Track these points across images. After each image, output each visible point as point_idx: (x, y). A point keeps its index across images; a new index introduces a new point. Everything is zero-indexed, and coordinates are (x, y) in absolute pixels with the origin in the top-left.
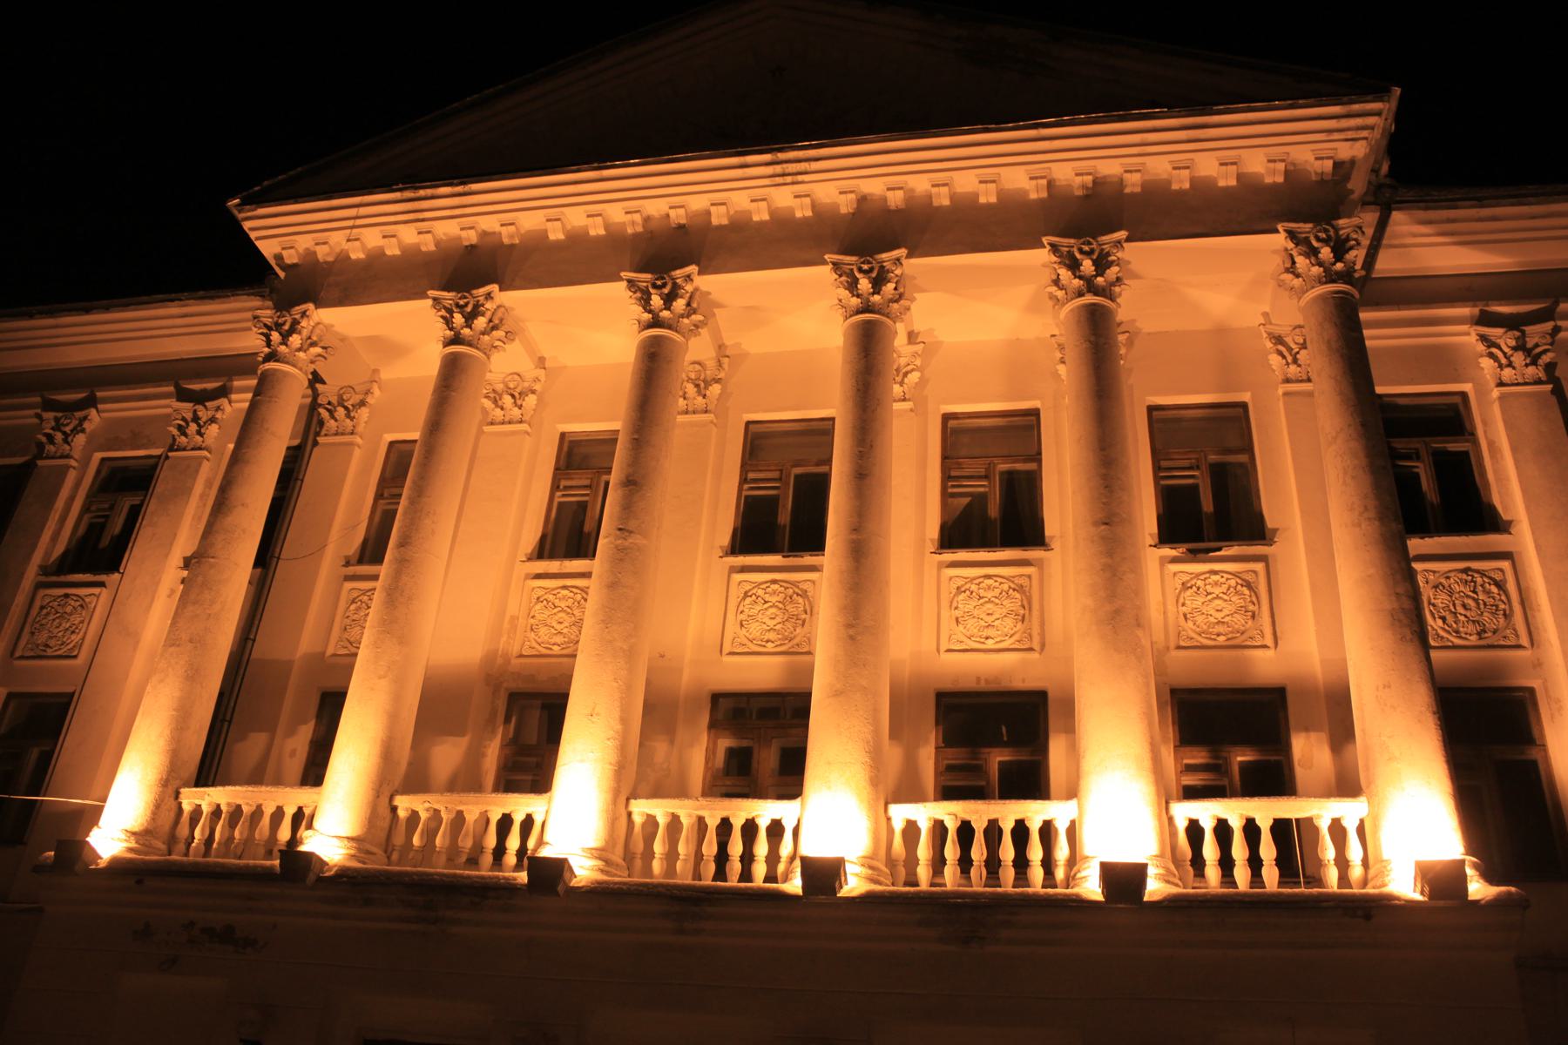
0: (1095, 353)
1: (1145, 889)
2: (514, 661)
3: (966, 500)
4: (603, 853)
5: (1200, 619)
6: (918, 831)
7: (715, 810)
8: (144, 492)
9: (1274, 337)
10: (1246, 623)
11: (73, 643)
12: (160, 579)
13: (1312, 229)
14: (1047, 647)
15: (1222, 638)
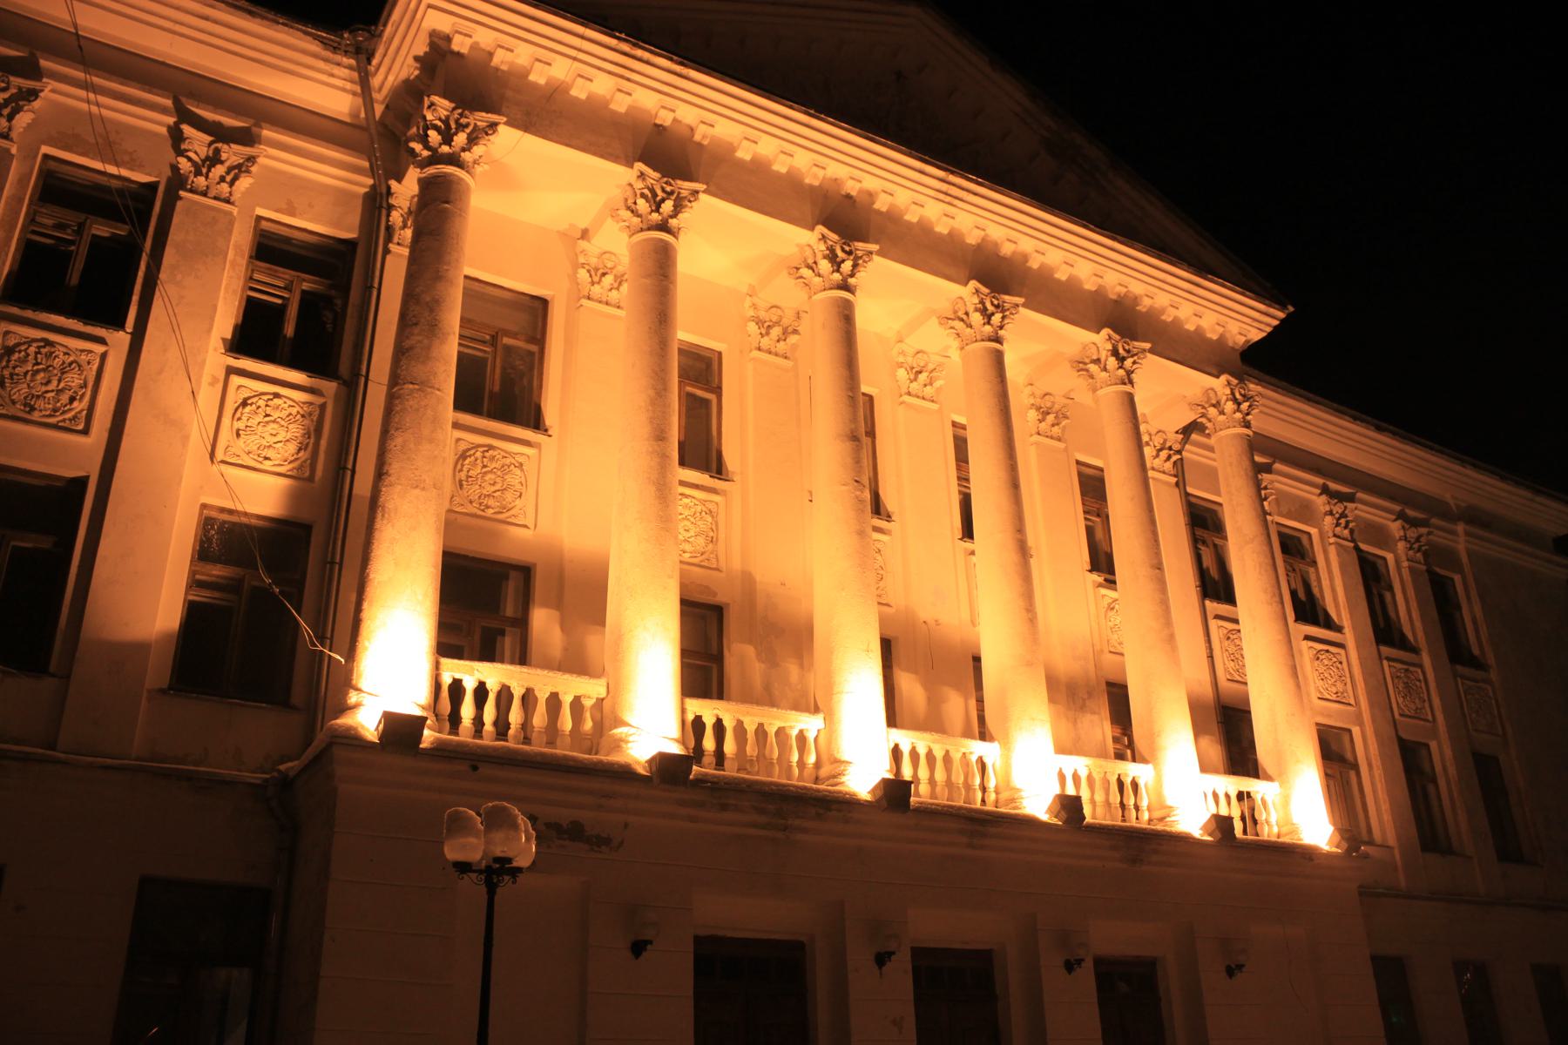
6: (703, 725)
11: (73, 413)
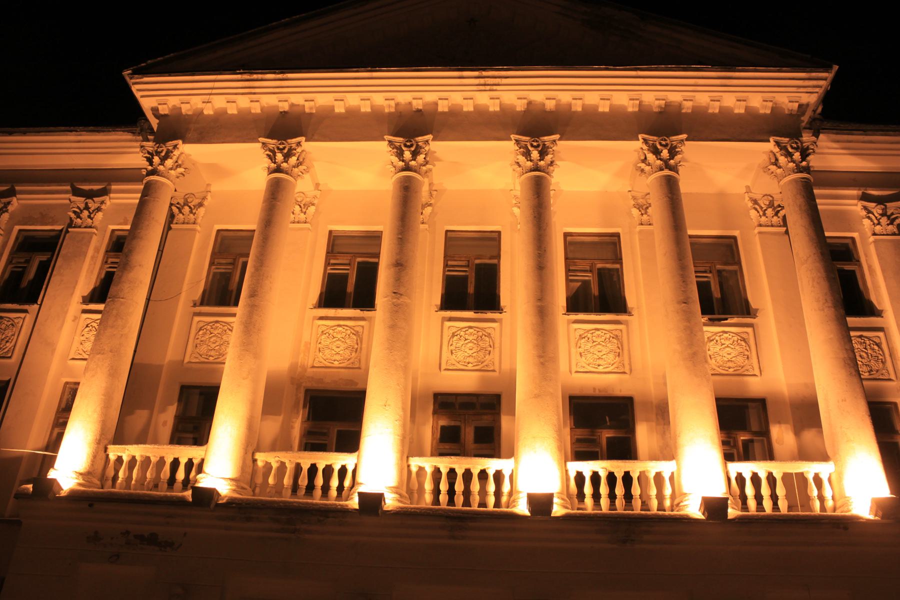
0: (671, 204)
1: (552, 509)
2: (310, 370)
3: (579, 284)
4: (398, 490)
5: (719, 358)
6: (615, 478)
7: (463, 464)
8: (50, 253)
9: (753, 200)
10: (744, 361)
12: (68, 310)
13: (789, 141)
14: (633, 371)
15: (731, 370)
